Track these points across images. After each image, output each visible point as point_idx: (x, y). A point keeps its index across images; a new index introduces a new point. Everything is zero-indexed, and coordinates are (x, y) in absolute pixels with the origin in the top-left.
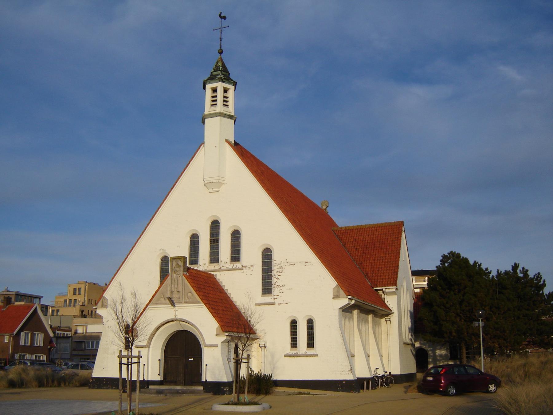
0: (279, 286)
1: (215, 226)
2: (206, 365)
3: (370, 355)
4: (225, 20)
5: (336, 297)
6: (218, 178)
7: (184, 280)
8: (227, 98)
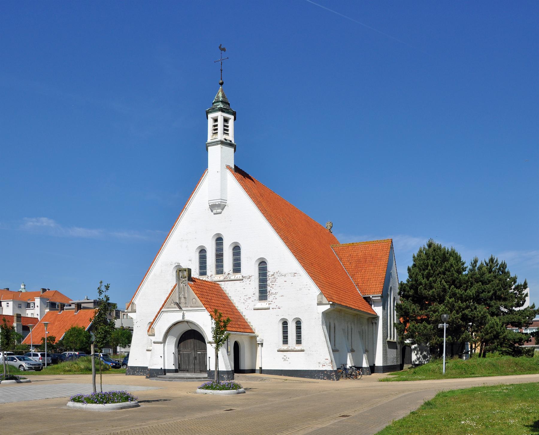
0: (273, 294)
1: (219, 240)
2: (209, 357)
4: (225, 52)
5: (320, 304)
6: (220, 200)
7: (189, 288)
8: (227, 127)
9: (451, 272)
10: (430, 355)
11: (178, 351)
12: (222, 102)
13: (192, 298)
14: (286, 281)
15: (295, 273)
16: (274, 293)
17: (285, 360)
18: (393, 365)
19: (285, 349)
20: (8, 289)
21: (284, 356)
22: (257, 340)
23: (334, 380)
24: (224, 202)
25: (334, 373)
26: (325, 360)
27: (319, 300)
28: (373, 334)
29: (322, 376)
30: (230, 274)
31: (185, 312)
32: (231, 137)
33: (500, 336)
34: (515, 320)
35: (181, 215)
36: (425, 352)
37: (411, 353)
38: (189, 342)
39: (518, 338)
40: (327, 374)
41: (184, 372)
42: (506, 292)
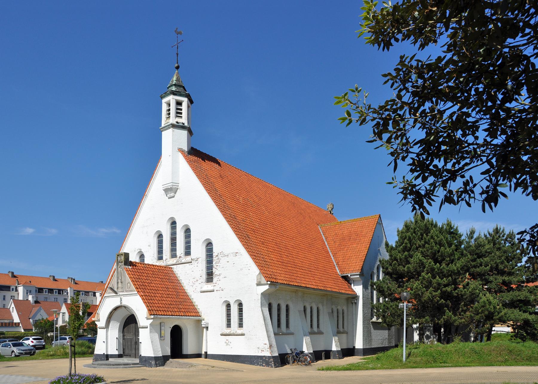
1: (173, 224)
3: (293, 332)
4: (181, 35)
5: (259, 284)
8: (181, 110)
9: (431, 245)
10: (434, 336)
11: (123, 336)
12: (175, 85)
13: (127, 282)
14: (228, 262)
15: (236, 253)
16: (218, 274)
17: (227, 344)
18: (383, 347)
19: (227, 333)
20: (102, 282)
21: (227, 340)
22: (202, 324)
23: (272, 367)
24: (175, 186)
25: (272, 360)
26: (263, 345)
27: (258, 281)
28: (353, 315)
29: (261, 362)
30: (181, 257)
31: (122, 297)
32: (184, 120)
33: (494, 316)
34: (520, 297)
35: (142, 202)
36: (428, 332)
37: (413, 333)
38: (131, 326)
39: (523, 320)
40: (265, 361)
41: (128, 357)
42: (510, 266)
